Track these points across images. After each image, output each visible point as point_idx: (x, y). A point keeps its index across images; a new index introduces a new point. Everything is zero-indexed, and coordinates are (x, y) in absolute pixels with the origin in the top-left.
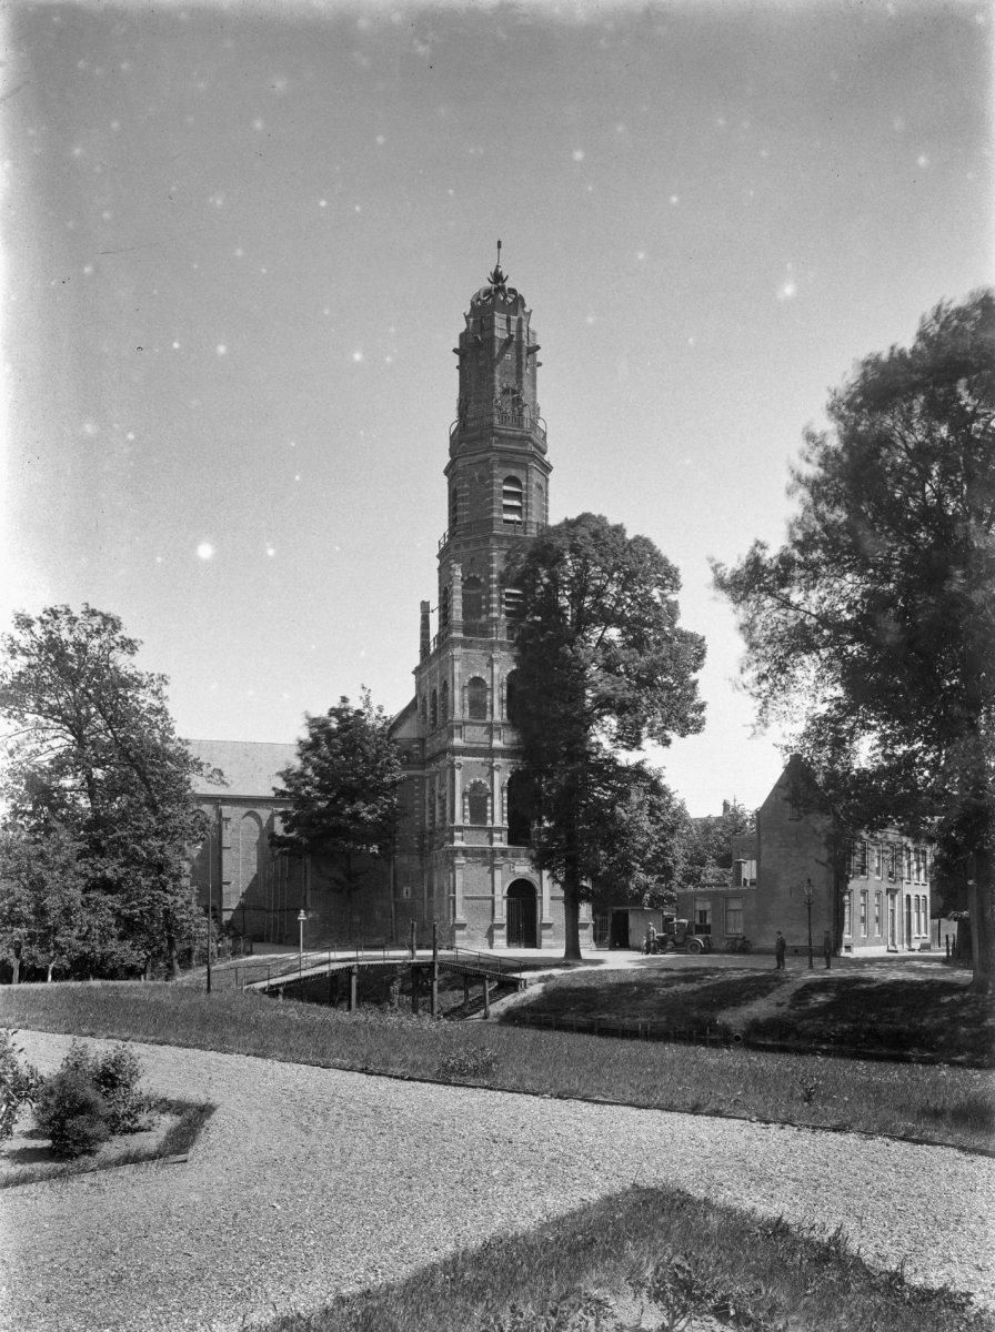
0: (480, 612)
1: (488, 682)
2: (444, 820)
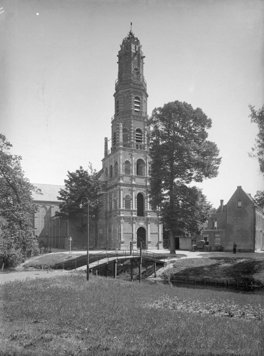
0: (127, 140)
1: (131, 163)
2: (116, 207)
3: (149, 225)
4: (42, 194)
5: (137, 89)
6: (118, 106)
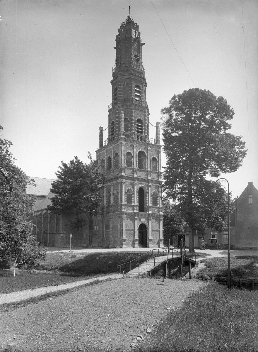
0: (128, 130)
1: (132, 154)
2: (116, 201)
3: (150, 222)
4: (35, 185)
5: (138, 77)
6: (117, 93)
